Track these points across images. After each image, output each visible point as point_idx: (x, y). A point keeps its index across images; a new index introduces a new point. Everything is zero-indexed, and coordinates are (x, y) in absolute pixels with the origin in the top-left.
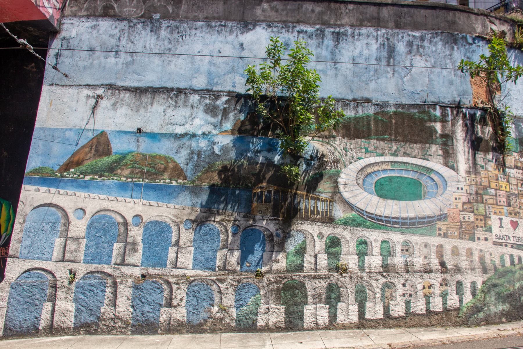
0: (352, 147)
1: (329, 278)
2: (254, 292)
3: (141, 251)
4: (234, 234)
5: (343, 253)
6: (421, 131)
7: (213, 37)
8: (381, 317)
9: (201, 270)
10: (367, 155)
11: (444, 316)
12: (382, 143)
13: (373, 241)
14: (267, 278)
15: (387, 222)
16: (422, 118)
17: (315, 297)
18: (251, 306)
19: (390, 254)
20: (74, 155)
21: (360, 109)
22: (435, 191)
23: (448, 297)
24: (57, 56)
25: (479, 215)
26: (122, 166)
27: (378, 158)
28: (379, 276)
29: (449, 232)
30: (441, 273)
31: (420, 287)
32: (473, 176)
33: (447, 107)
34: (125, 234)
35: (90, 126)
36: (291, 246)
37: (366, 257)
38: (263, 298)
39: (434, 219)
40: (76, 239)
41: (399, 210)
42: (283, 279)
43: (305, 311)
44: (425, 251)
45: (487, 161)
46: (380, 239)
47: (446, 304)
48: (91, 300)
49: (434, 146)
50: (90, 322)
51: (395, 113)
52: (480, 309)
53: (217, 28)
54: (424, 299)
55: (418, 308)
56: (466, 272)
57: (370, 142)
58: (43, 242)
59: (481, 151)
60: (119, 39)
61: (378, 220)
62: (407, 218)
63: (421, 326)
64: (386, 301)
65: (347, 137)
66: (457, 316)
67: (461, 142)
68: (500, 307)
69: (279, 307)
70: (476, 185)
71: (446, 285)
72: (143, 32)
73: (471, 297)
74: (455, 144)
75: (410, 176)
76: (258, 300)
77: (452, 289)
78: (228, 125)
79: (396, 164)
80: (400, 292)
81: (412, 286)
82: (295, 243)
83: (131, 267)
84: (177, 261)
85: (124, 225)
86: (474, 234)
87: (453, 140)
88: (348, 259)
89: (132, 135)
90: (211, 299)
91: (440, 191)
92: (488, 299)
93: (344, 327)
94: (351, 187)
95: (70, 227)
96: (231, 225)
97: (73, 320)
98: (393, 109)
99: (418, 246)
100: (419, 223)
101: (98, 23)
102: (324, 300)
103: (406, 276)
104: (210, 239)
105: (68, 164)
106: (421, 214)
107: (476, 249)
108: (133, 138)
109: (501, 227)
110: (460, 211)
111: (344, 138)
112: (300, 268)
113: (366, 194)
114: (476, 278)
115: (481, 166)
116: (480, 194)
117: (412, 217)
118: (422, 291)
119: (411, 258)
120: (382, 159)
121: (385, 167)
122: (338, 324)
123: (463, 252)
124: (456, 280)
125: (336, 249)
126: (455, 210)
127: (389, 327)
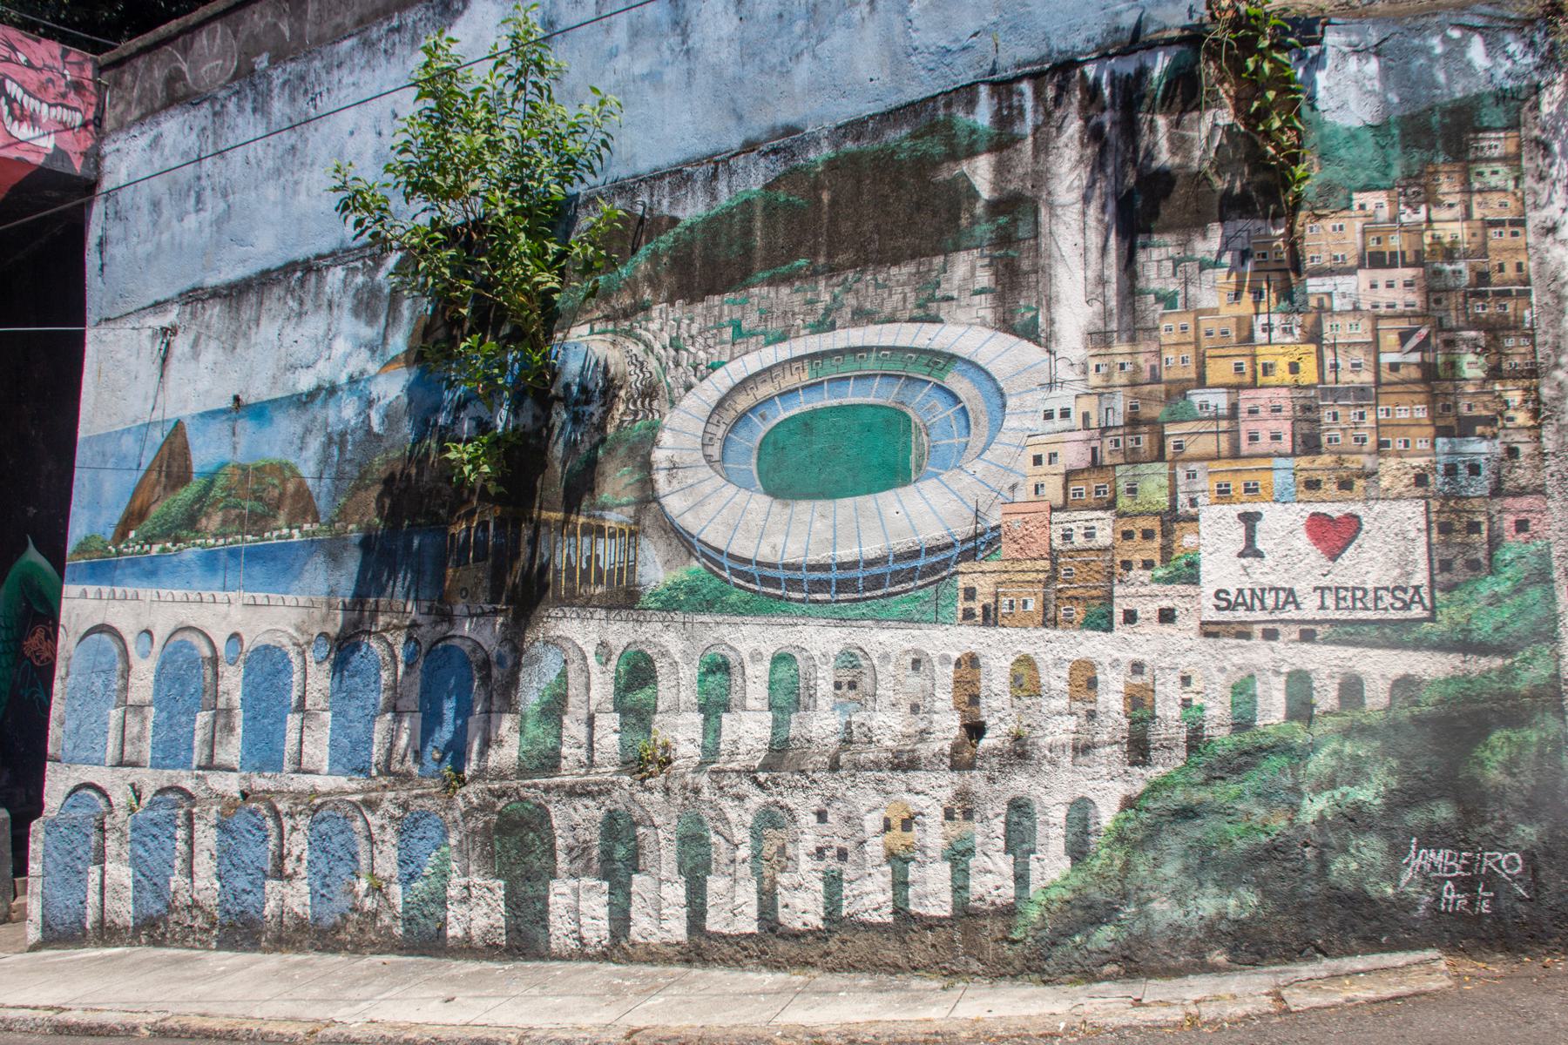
0: (694, 330)
1: (609, 792)
2: (437, 840)
3: (239, 730)
4: (409, 666)
5: (661, 707)
6: (919, 207)
7: (378, 72)
8: (753, 928)
9: (344, 774)
10: (737, 349)
11: (958, 936)
12: (785, 291)
13: (747, 659)
14: (464, 796)
15: (794, 584)
16: (925, 153)
17: (574, 854)
18: (433, 879)
19: (798, 702)
21: (722, 186)
22: (958, 441)
23: (972, 862)
24: (102, 244)
25: (1141, 514)
27: (771, 349)
28: (746, 786)
29: (1005, 601)
30: (952, 768)
31: (872, 823)
32: (1121, 347)
33: (1018, 79)
35: (157, 415)
36: (531, 696)
37: (726, 717)
38: (456, 855)
39: (948, 553)
40: (139, 708)
41: (830, 535)
42: (499, 797)
43: (552, 899)
44: (915, 682)
45: (1192, 268)
46: (769, 650)
47: (965, 888)
49: (963, 255)
51: (831, 164)
52: (1101, 912)
53: (382, 45)
54: (888, 869)
55: (866, 901)
56: (1053, 763)
57: (749, 296)
59: (1167, 229)
61: (766, 581)
62: (854, 565)
63: (875, 967)
64: (767, 872)
65: (682, 297)
66: (1005, 939)
67: (1071, 215)
68: (1203, 902)
69: (490, 883)
70: (1133, 384)
71: (968, 815)
72: (240, 121)
73: (1067, 862)
74: (1044, 230)
75: (870, 400)
76: (445, 861)
77: (990, 830)
78: (399, 342)
79: (827, 362)
80: (810, 842)
81: (848, 819)
82: (540, 681)
83: (223, 774)
84: (301, 752)
86: (1109, 598)
87: (1036, 212)
88: (675, 727)
90: (354, 857)
91: (977, 440)
92: (1143, 870)
93: (652, 956)
94: (689, 473)
96: (402, 639)
97: (131, 908)
98: (827, 151)
99: (891, 668)
100: (898, 577)
102: (596, 865)
103: (829, 782)
104: (360, 687)
106: (902, 544)
107: (1115, 663)
109: (1250, 550)
110: (1053, 509)
111: (673, 305)
112: (550, 762)
113: (730, 490)
114: (1091, 784)
115: (1160, 298)
116: (1152, 422)
117: (872, 556)
118: (879, 840)
119: (864, 714)
120: (783, 352)
121: (790, 380)
122: (634, 945)
123: (1055, 679)
124: (1009, 795)
125: (642, 695)
126: (1032, 507)
127: (776, 966)
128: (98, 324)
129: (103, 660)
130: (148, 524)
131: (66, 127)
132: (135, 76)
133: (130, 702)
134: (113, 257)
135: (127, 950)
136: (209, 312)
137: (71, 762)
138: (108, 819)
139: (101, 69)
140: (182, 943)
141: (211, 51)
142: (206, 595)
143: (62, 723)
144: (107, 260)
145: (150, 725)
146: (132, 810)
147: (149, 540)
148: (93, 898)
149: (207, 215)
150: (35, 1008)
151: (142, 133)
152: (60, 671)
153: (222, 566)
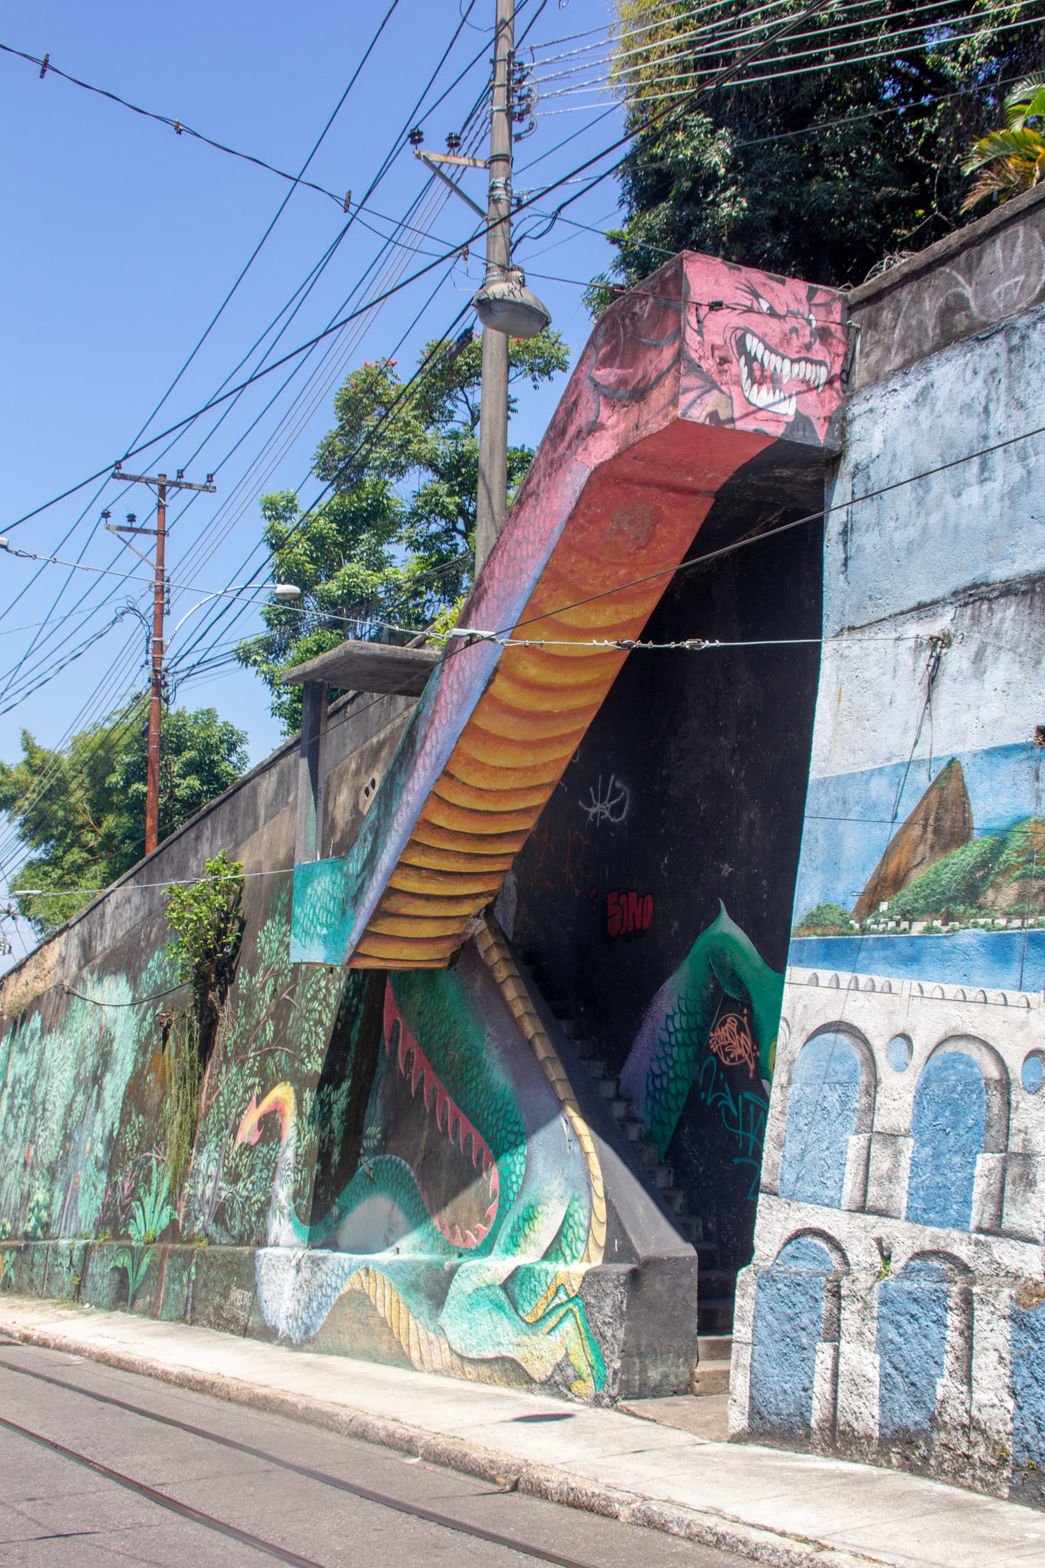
20: (887, 856)
24: (846, 532)
26: (997, 874)
34: (1004, 1122)
35: (922, 752)
40: (891, 1137)
48: (912, 1351)
50: (912, 1428)
58: (824, 1145)
60: (986, 410)
83: (1018, 1244)
85: (1002, 1087)
89: (1022, 756)
95: (878, 1098)
97: (876, 1411)
101: (930, 378)
105: (876, 888)
108: (1025, 766)
128: (839, 634)
129: (839, 1068)
130: (906, 895)
131: (809, 387)
132: (897, 312)
133: (877, 1127)
134: (860, 549)
135: (875, 1471)
136: (998, 616)
137: (792, 1197)
138: (845, 1282)
139: (851, 309)
140: (955, 1477)
141: (1007, 264)
142: (992, 995)
143: (781, 1145)
144: (852, 552)
145: (905, 1162)
146: (879, 1276)
147: (909, 915)
148: (821, 1387)
149: (996, 487)
150: (783, 1534)
151: (905, 386)
152: (779, 1077)
153: (1017, 956)
